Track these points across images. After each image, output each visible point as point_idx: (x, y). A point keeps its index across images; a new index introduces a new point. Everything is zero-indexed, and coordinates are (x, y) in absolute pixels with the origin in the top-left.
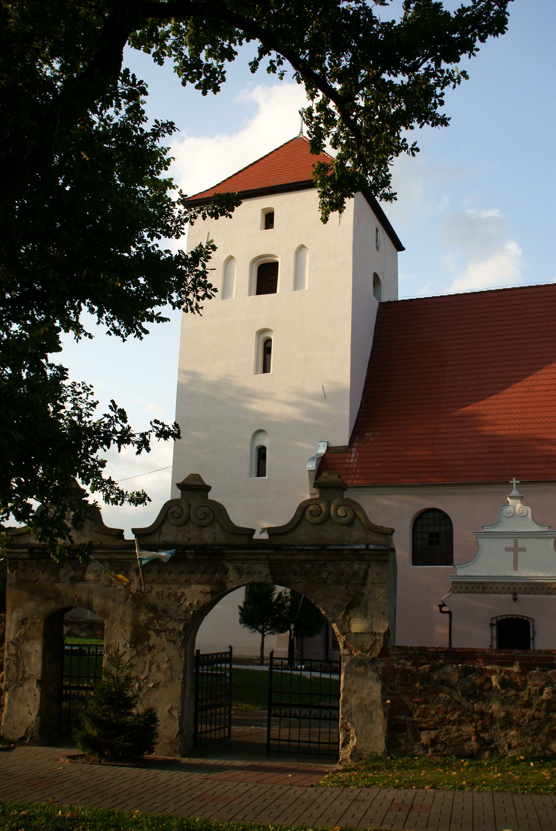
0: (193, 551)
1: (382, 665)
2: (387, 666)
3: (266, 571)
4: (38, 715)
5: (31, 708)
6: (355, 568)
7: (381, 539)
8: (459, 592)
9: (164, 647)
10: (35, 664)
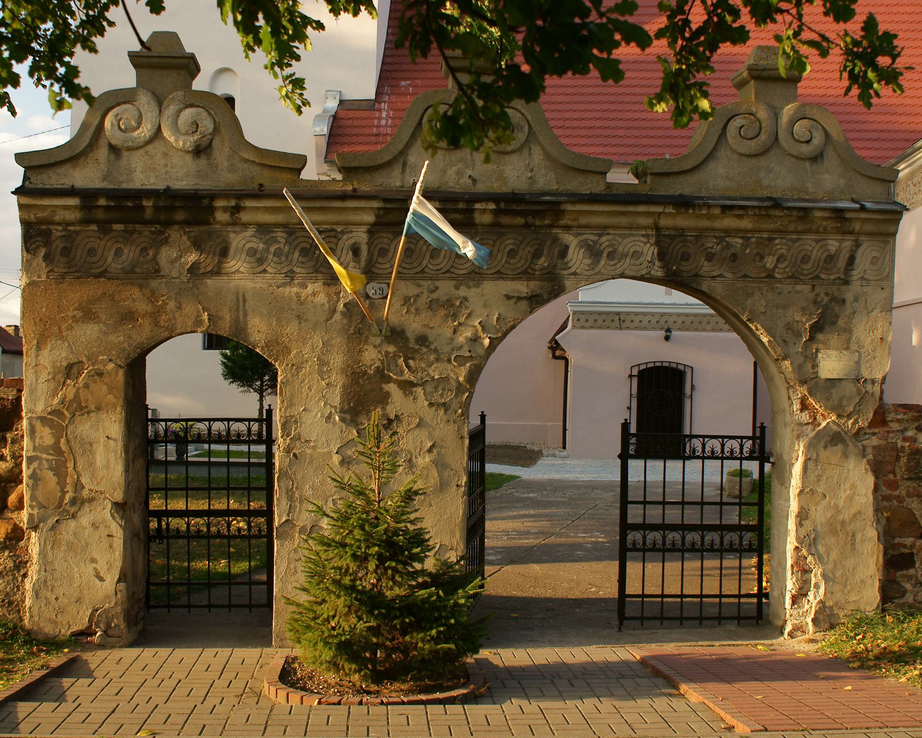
0: (492, 206)
1: (875, 441)
2: (884, 442)
3: (650, 253)
4: (119, 581)
5: (102, 566)
6: (831, 248)
7: (877, 189)
8: (583, 327)
9: (421, 419)
10: (107, 466)
